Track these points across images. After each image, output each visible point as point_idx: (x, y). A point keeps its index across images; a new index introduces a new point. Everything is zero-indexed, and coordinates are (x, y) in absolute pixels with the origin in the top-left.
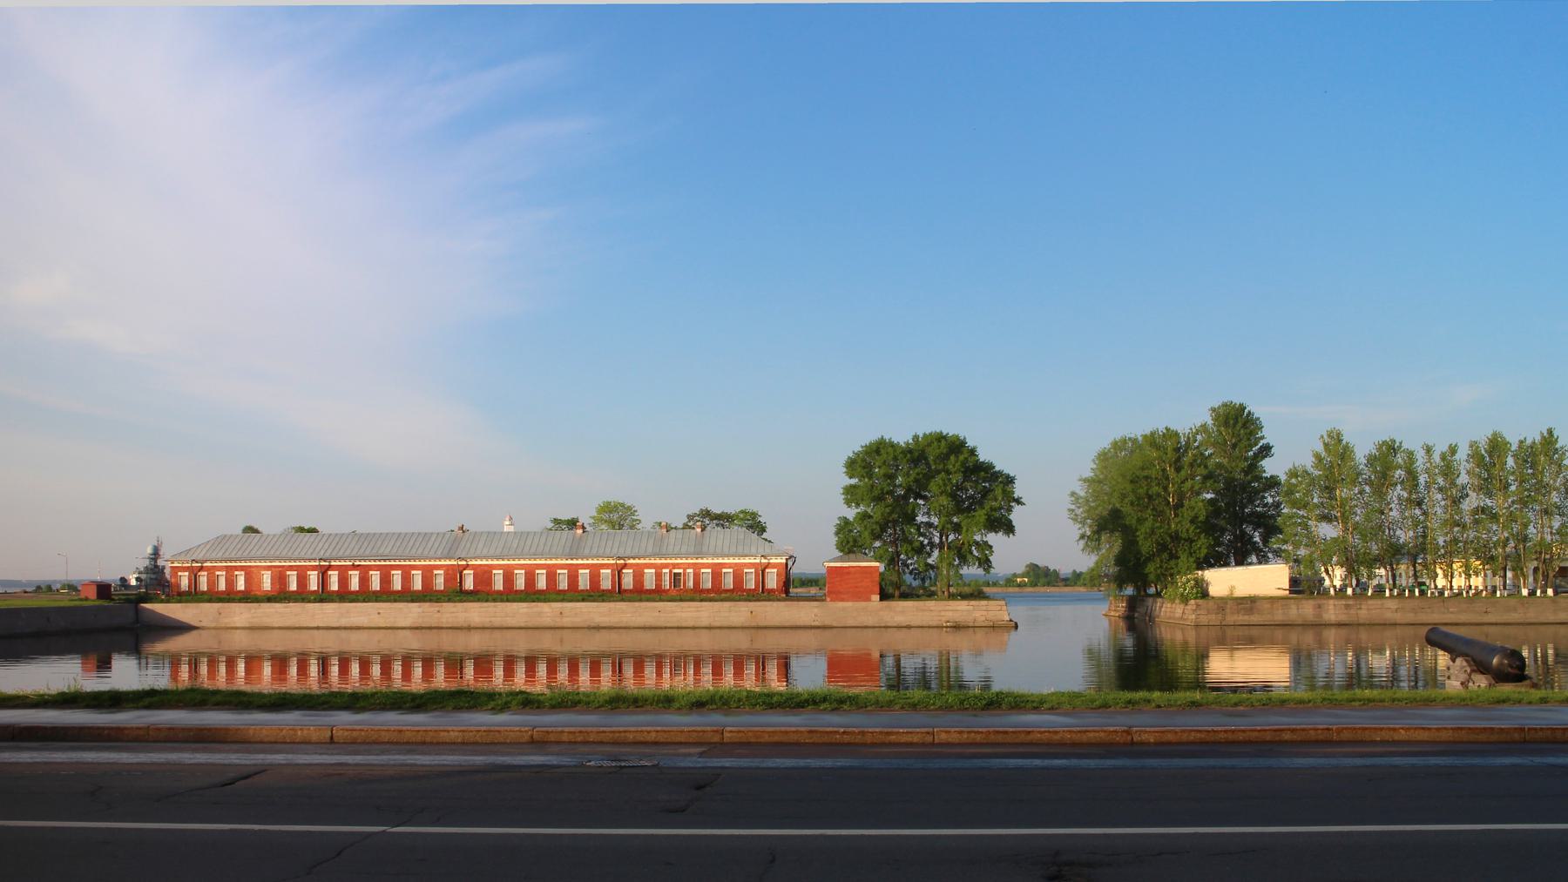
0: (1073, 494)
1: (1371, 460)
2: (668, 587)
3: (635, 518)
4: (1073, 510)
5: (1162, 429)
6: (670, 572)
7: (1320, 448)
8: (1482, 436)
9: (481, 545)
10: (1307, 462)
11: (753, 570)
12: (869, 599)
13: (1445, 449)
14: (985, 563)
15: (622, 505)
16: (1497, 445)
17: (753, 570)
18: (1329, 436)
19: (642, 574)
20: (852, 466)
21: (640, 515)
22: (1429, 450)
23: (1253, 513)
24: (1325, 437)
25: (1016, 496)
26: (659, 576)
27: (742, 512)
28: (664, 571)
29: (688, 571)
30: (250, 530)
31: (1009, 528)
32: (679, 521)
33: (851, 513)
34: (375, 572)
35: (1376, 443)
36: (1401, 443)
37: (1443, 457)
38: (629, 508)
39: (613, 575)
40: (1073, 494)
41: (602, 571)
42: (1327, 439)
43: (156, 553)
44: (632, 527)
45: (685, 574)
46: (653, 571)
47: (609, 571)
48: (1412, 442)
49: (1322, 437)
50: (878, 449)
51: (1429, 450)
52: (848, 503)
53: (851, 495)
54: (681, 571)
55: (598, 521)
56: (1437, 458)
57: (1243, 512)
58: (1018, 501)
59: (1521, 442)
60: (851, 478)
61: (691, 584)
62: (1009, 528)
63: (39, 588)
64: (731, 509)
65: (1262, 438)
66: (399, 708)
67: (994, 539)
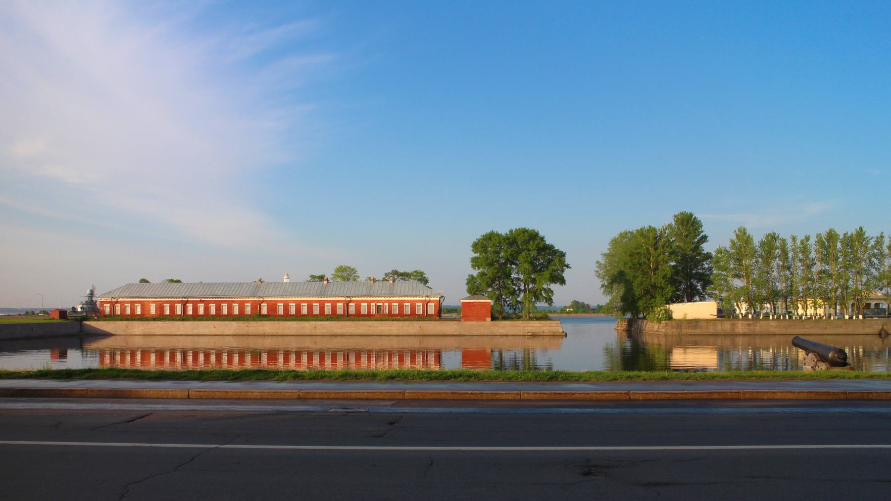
1: (762, 244)
2: (374, 313)
3: (356, 275)
4: (598, 271)
5: (647, 227)
6: (376, 305)
7: (734, 237)
8: (824, 232)
9: (271, 290)
11: (421, 304)
12: (485, 320)
13: (803, 238)
14: (549, 300)
15: (349, 268)
16: (832, 236)
17: (421, 304)
18: (739, 231)
19: (360, 306)
21: (359, 273)
22: (794, 239)
23: (697, 273)
24: (737, 231)
26: (369, 307)
27: (415, 272)
28: (372, 304)
30: (144, 281)
31: (562, 281)
32: (380, 277)
33: (475, 273)
35: (765, 235)
36: (778, 235)
37: (802, 242)
38: (353, 270)
39: (344, 307)
40: (598, 262)
41: (338, 304)
43: (92, 294)
44: (354, 280)
45: (383, 306)
46: (366, 304)
47: (342, 304)
48: (784, 234)
49: (735, 231)
50: (490, 237)
51: (794, 239)
52: (474, 267)
53: (475, 262)
54: (381, 304)
55: (336, 276)
56: (798, 243)
57: (692, 273)
58: (568, 266)
59: (845, 234)
60: (475, 253)
61: (168, 312)
62: (562, 281)
63: (27, 313)
64: (409, 270)
65: (702, 232)
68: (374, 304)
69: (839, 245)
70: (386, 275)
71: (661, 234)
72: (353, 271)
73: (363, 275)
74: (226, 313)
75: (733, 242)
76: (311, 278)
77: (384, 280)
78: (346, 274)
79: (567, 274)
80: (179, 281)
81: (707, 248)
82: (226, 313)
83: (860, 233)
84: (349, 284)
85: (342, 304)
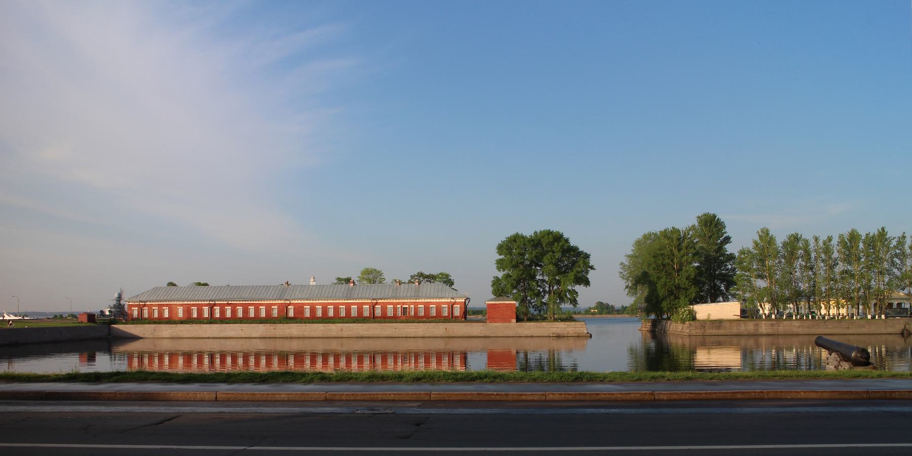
0: (622, 264)
1: (785, 245)
5: (670, 228)
6: (401, 307)
7: (757, 238)
10: (750, 246)
14: (574, 302)
15: (375, 270)
18: (762, 231)
21: (385, 276)
22: (816, 239)
23: (720, 274)
24: (760, 232)
25: (590, 265)
26: (395, 309)
28: (398, 306)
29: (411, 306)
30: (171, 284)
31: (587, 283)
32: (406, 279)
37: (824, 243)
38: (379, 272)
40: (622, 264)
42: (761, 234)
44: (380, 282)
49: (758, 232)
50: (515, 239)
51: (816, 239)
52: (499, 269)
53: (500, 264)
54: (407, 306)
55: (362, 279)
56: (821, 243)
58: (592, 268)
59: (867, 235)
61: (195, 315)
62: (587, 283)
64: (435, 272)
65: (725, 233)
66: (253, 382)
67: (579, 288)
68: (400, 306)
69: (861, 245)
70: (412, 277)
71: (684, 235)
72: (379, 273)
73: (388, 278)
74: (253, 316)
75: (756, 243)
76: (337, 281)
77: (410, 282)
78: (372, 277)
79: (591, 275)
80: (206, 285)
81: (730, 249)
82: (253, 316)
83: (882, 233)
84: (375, 287)
85: (368, 306)
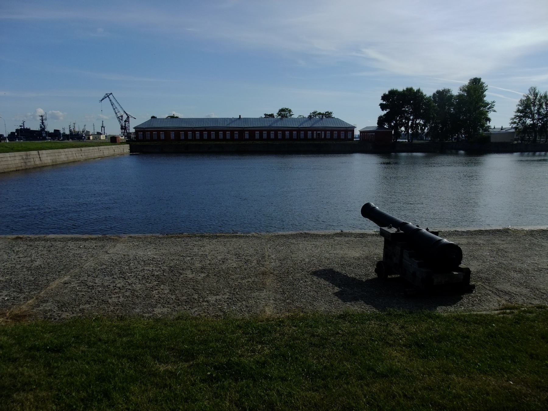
6: (317, 132)
19: (270, 133)
20: (384, 97)
26: (313, 134)
28: (314, 132)
29: (323, 132)
34: (236, 132)
52: (383, 110)
61: (323, 137)
68: (316, 132)
85: (296, 132)
